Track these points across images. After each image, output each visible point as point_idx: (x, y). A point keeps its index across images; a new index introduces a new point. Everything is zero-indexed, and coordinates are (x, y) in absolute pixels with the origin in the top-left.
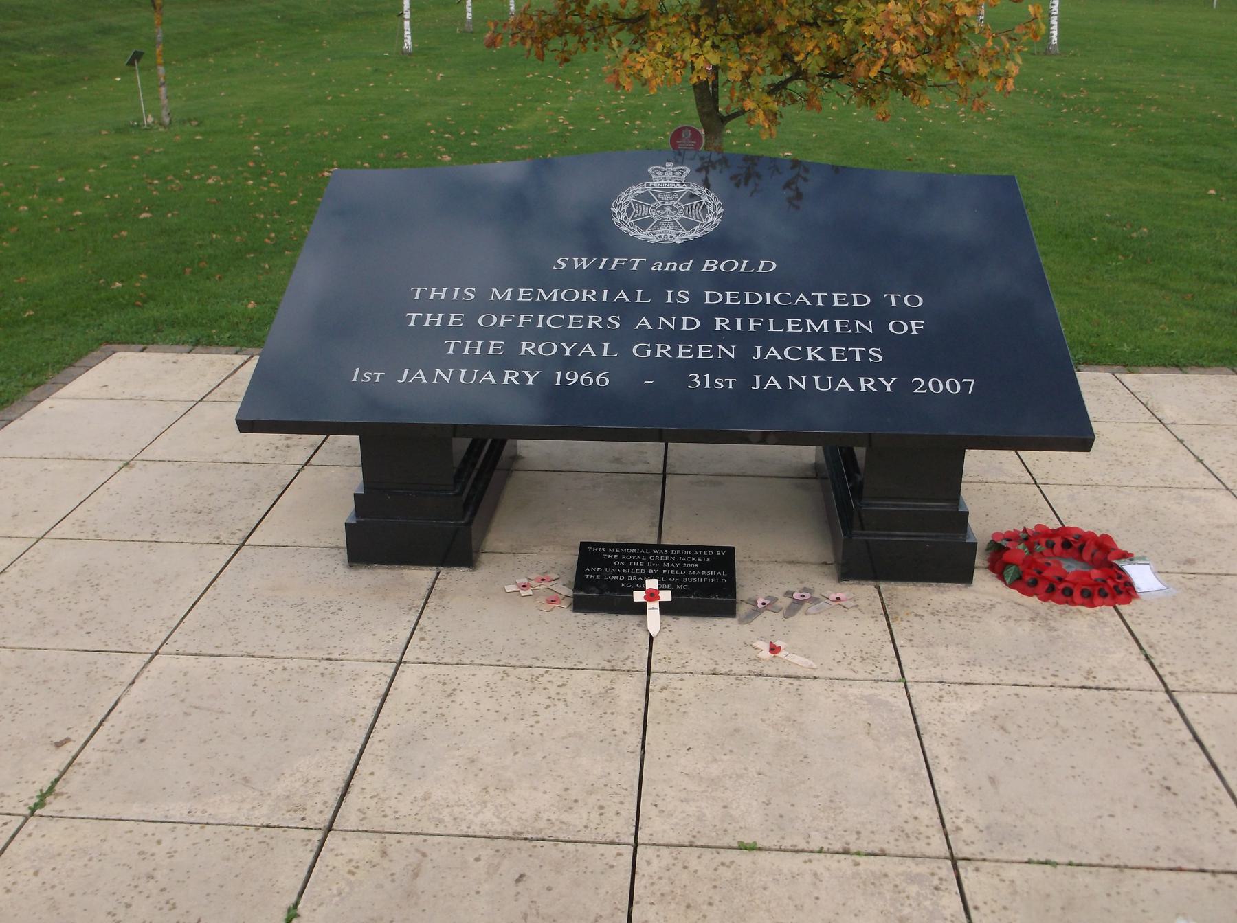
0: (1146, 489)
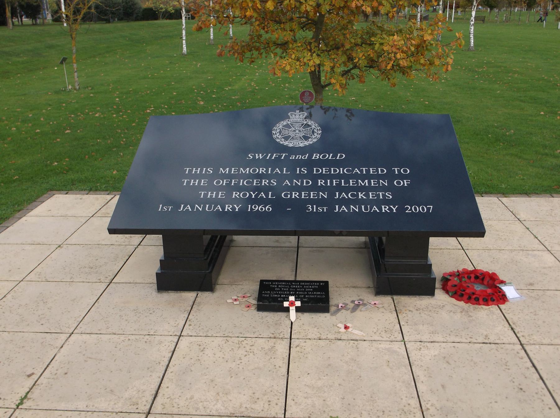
0: (512, 251)
